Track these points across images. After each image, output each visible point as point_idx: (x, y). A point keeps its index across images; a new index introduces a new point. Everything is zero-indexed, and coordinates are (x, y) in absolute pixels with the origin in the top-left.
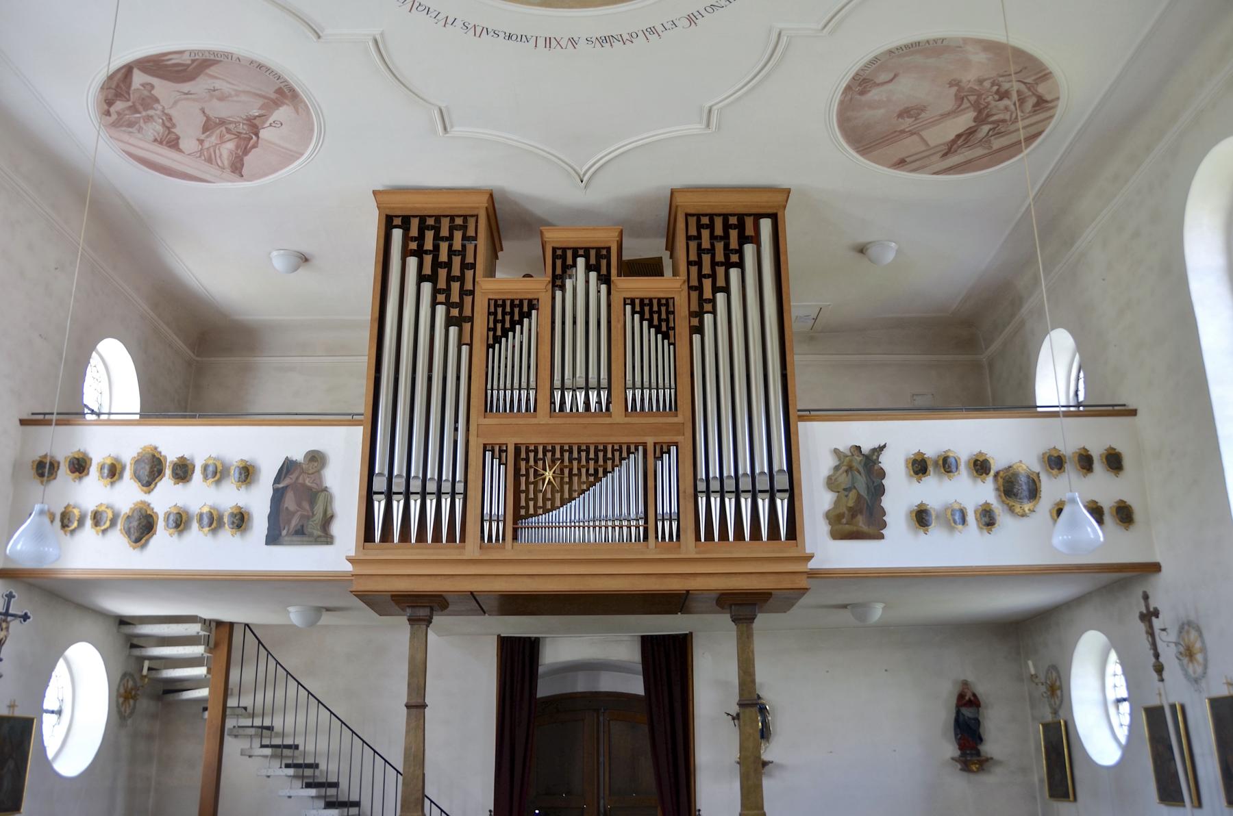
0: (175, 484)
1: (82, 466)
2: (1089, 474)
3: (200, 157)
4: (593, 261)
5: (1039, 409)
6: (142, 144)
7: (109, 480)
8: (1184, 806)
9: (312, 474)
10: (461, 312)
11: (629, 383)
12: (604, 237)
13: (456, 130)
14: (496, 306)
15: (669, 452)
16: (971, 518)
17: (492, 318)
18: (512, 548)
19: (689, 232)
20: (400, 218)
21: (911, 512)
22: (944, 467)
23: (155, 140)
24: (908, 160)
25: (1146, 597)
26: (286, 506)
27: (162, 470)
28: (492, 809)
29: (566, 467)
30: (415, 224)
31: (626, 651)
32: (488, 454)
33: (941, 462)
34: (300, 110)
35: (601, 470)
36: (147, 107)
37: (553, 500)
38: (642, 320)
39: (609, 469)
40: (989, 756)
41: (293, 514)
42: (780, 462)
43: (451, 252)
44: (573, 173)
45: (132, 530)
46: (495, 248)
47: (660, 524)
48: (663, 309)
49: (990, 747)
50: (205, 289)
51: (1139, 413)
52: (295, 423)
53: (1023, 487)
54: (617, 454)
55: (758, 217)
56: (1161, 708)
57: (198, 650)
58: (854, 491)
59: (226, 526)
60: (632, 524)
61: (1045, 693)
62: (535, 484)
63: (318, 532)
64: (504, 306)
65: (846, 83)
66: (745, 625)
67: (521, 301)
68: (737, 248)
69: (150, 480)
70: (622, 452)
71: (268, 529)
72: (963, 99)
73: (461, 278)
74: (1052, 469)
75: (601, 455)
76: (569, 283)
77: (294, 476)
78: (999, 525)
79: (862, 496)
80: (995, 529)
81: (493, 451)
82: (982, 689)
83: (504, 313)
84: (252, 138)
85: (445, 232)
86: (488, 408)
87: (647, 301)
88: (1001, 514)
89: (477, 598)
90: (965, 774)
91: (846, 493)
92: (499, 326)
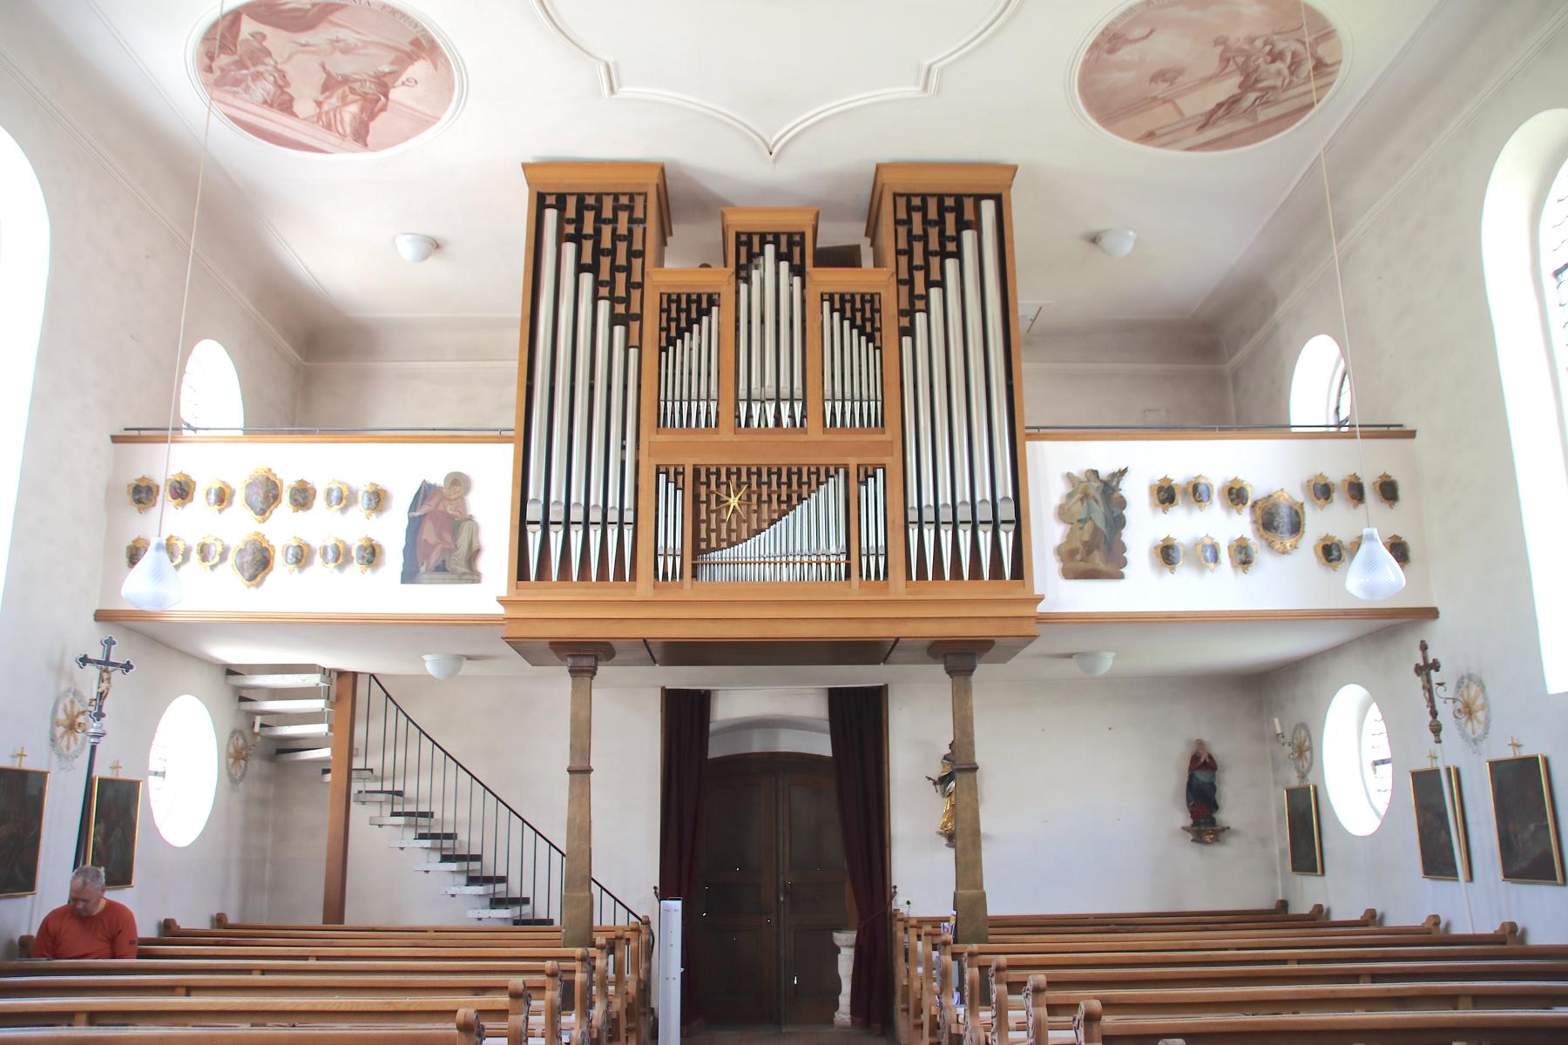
0: (294, 512)
1: (185, 491)
2: (1326, 506)
3: (318, 122)
4: (784, 249)
5: (1294, 430)
6: (249, 107)
7: (217, 507)
8: (1457, 880)
9: (455, 500)
10: (628, 308)
11: (828, 394)
12: (802, 222)
13: (625, 91)
14: (670, 301)
15: (875, 476)
16: (1224, 555)
17: (664, 316)
18: (692, 588)
19: (898, 215)
20: (554, 197)
21: (1156, 548)
22: (1194, 495)
23: (265, 102)
24: (1158, 133)
25: (1424, 647)
26: (424, 537)
27: (278, 495)
28: (658, 886)
29: (754, 492)
30: (572, 203)
31: (814, 707)
32: (662, 477)
33: (1191, 490)
34: (439, 65)
35: (795, 496)
36: (256, 61)
37: (738, 531)
38: (842, 319)
39: (805, 495)
40: (1225, 825)
41: (433, 547)
42: (1005, 488)
43: (616, 237)
44: (761, 143)
45: (245, 566)
46: (665, 233)
47: (864, 560)
48: (868, 306)
49: (1227, 815)
50: (316, 281)
51: (1418, 434)
52: (386, 439)
53: (1284, 519)
54: (814, 478)
55: (979, 198)
56: (1436, 772)
57: (318, 704)
58: (1090, 523)
59: (355, 561)
60: (832, 560)
61: (1292, 754)
62: (718, 512)
63: (462, 569)
64: (678, 301)
65: (1093, 39)
66: (962, 677)
67: (699, 296)
68: (954, 234)
69: (264, 507)
70: (821, 475)
71: (404, 565)
72: (1229, 61)
73: (628, 269)
74: (1319, 499)
75: (795, 478)
76: (755, 275)
77: (433, 503)
78: (1256, 564)
79: (1099, 529)
80: (1251, 568)
81: (667, 473)
82: (1218, 749)
83: (679, 310)
84: (380, 99)
85: (607, 213)
86: (661, 422)
87: (848, 297)
88: (1259, 551)
89: (651, 646)
90: (1198, 845)
91: (1081, 525)
92: (673, 325)
